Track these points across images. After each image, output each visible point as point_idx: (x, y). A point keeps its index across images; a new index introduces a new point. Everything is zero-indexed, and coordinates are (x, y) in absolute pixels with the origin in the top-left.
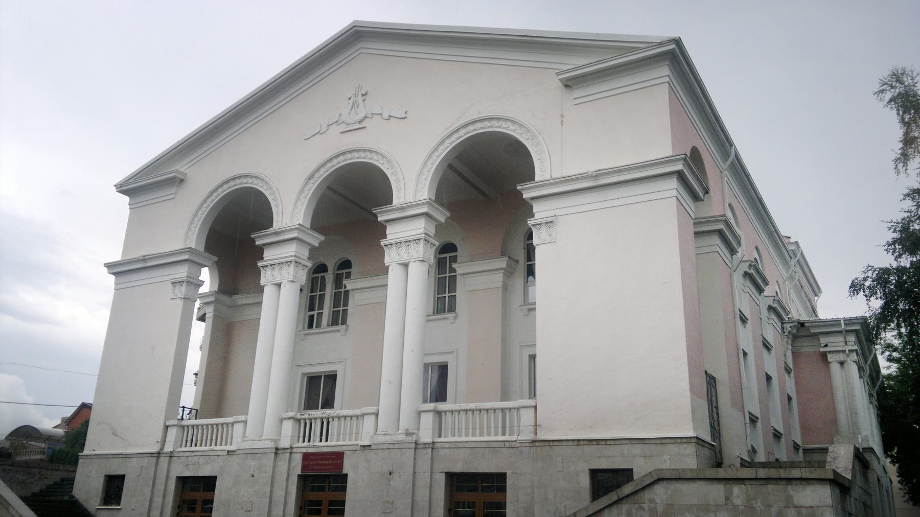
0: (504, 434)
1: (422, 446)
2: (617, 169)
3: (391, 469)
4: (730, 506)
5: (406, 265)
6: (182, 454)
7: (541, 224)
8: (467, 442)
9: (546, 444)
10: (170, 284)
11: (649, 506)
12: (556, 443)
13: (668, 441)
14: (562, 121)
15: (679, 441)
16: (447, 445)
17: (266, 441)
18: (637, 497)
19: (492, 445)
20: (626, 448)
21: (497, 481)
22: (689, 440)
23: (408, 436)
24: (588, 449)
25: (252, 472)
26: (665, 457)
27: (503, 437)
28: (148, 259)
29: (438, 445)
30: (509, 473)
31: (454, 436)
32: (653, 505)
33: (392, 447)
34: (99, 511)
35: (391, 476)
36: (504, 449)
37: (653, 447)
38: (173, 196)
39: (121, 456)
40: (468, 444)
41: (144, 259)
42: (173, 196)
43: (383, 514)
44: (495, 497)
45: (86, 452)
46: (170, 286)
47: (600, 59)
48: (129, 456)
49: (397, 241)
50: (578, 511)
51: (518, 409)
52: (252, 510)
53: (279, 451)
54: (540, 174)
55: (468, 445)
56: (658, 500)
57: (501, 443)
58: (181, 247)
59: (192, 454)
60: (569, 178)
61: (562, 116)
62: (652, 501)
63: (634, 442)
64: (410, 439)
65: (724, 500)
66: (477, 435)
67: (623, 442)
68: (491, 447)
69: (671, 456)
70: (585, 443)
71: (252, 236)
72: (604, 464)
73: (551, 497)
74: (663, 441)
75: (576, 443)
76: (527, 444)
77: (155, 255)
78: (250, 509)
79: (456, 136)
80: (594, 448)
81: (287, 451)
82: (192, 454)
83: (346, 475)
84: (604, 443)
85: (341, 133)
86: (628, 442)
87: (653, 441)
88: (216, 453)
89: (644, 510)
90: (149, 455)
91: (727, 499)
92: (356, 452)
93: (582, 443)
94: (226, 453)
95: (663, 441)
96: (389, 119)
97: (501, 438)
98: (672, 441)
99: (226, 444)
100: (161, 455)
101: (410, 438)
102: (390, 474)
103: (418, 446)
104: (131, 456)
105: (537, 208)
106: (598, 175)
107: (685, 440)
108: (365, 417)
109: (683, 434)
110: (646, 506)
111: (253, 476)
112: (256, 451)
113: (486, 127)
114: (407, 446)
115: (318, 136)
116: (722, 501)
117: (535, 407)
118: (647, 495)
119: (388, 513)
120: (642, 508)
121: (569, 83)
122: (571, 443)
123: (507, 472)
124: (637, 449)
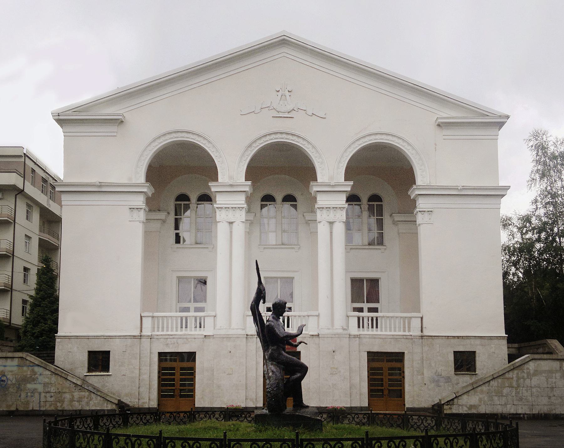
0: (390, 331)
1: (352, 336)
2: (473, 187)
3: (334, 349)
4: (562, 371)
5: (331, 223)
6: (161, 337)
7: (323, 208)
8: (380, 335)
9: (430, 338)
10: (128, 209)
11: (527, 371)
12: (435, 338)
13: (494, 338)
14: (436, 148)
15: (499, 338)
16: (368, 336)
17: (238, 330)
18: (521, 367)
19: (396, 337)
20: (472, 341)
21: (399, 357)
22: (504, 338)
23: (345, 331)
24: (453, 341)
25: (229, 349)
26: (492, 346)
27: (390, 332)
28: (104, 186)
29: (361, 336)
30: (406, 352)
31: (400, 331)
32: (528, 371)
33: (334, 336)
34: (88, 377)
35: (335, 353)
36: (402, 339)
37: (486, 341)
38: (115, 134)
39: (103, 337)
40: (381, 336)
41: (101, 185)
42: (115, 134)
43: (331, 375)
44: (398, 365)
45: (59, 334)
46: (128, 211)
47: (465, 116)
48: (111, 337)
49: (327, 206)
50: (494, 373)
51: (411, 318)
52: (233, 374)
53: (248, 337)
54: (320, 179)
55: (381, 337)
56: (531, 368)
57: (401, 336)
58: (125, 181)
59: (171, 337)
60: (339, 184)
61: (436, 145)
62: (528, 369)
63: (476, 338)
64: (345, 332)
65: (559, 368)
66: (383, 331)
67: (471, 338)
68: (396, 338)
69: (495, 345)
70: (452, 338)
71: (209, 184)
72: (461, 349)
73: (433, 365)
74: (492, 338)
75: (446, 338)
76: (418, 337)
77: (65, 184)
78: (231, 373)
79: (163, 138)
80: (456, 340)
81: (254, 336)
82: (171, 337)
83: (300, 352)
84: (461, 338)
85: (272, 117)
86: (474, 338)
87: (487, 338)
88: (193, 337)
89: (524, 372)
90: (132, 337)
91: (560, 367)
92: (305, 338)
93: (450, 338)
94: (203, 337)
95: (492, 338)
96: (312, 116)
97: (402, 333)
98: (495, 338)
99: (167, 331)
100: (142, 337)
101: (346, 332)
102: (334, 352)
103: (351, 336)
104: (113, 337)
105: (319, 197)
106: (464, 188)
107: (502, 338)
108: (310, 317)
109: (492, 334)
110: (525, 371)
111: (230, 352)
112: (230, 336)
113: (395, 141)
114: (346, 336)
115: (253, 114)
116: (558, 368)
117: (422, 318)
118: (526, 366)
119: (334, 374)
120: (524, 372)
121: (441, 125)
122: (444, 337)
123: (405, 351)
124: (478, 342)
